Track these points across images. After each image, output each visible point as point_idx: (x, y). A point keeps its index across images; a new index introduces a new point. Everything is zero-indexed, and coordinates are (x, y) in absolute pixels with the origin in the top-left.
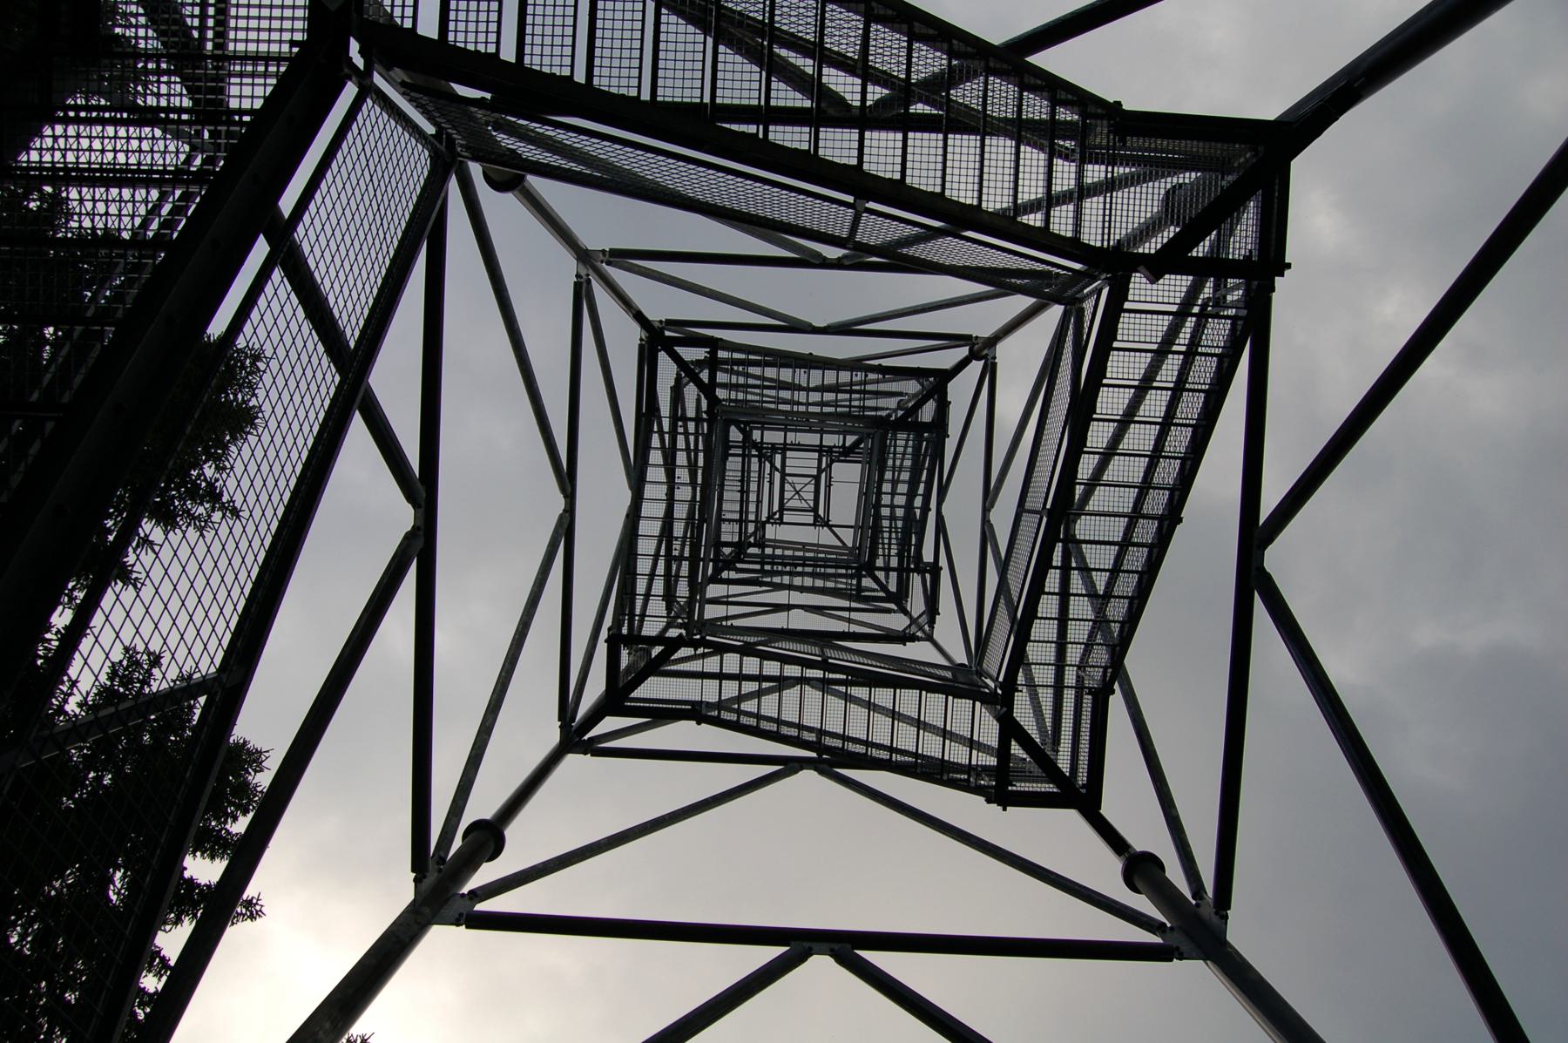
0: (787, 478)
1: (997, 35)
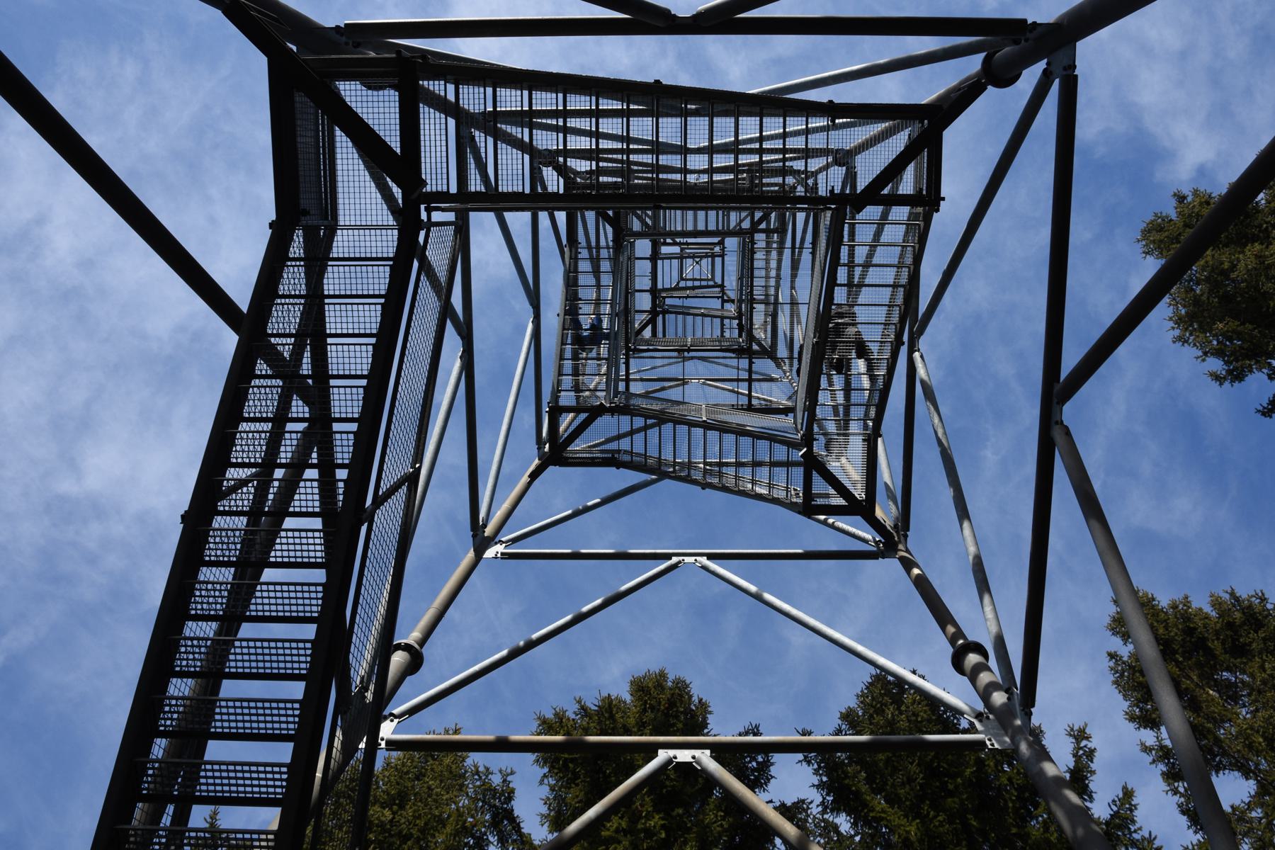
0: (731, 228)
1: (230, 340)
